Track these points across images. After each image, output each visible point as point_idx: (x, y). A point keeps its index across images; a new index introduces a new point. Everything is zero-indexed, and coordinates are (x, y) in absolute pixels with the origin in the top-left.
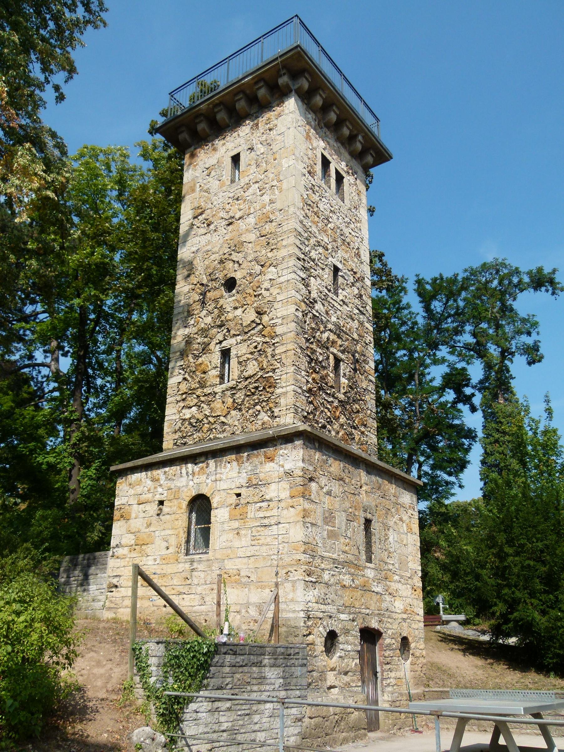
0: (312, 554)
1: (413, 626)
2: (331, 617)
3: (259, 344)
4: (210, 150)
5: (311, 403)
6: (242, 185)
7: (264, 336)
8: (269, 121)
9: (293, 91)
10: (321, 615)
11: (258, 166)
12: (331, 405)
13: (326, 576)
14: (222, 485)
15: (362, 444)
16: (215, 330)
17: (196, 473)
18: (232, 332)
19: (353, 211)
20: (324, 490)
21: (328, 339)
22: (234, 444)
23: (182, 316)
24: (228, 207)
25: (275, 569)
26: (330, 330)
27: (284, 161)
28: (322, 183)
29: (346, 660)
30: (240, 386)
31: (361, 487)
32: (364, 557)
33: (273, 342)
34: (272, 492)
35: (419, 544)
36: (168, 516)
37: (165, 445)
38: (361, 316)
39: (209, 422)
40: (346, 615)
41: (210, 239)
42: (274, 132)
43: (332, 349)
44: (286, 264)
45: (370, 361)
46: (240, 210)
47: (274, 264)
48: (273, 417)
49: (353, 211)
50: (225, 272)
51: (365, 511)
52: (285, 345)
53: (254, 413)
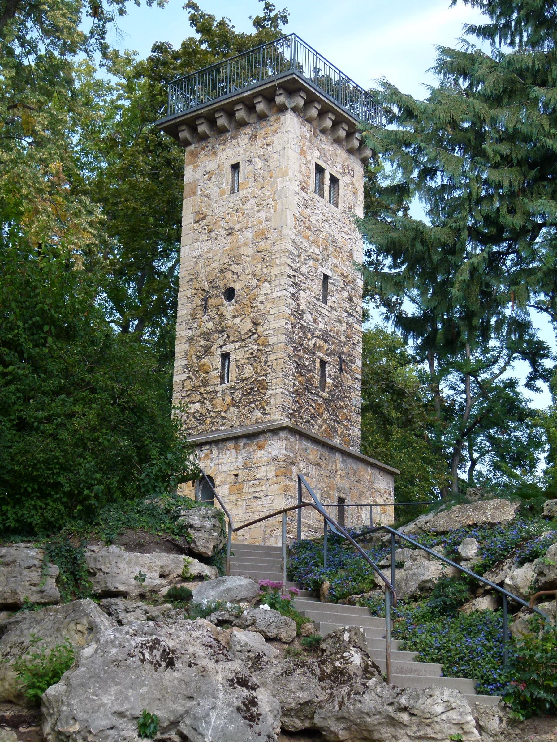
4: (211, 152)
5: (297, 402)
7: (259, 344)
8: (266, 136)
12: (315, 403)
14: (224, 468)
15: (344, 437)
17: (202, 459)
18: (232, 338)
22: (233, 435)
23: (186, 318)
25: (263, 529)
26: (317, 337)
27: (279, 180)
28: (317, 196)
31: (336, 472)
34: (262, 472)
38: (350, 319)
39: (211, 417)
41: (211, 246)
43: (318, 354)
46: (239, 222)
47: (268, 280)
48: (265, 414)
50: (226, 281)
51: (339, 491)
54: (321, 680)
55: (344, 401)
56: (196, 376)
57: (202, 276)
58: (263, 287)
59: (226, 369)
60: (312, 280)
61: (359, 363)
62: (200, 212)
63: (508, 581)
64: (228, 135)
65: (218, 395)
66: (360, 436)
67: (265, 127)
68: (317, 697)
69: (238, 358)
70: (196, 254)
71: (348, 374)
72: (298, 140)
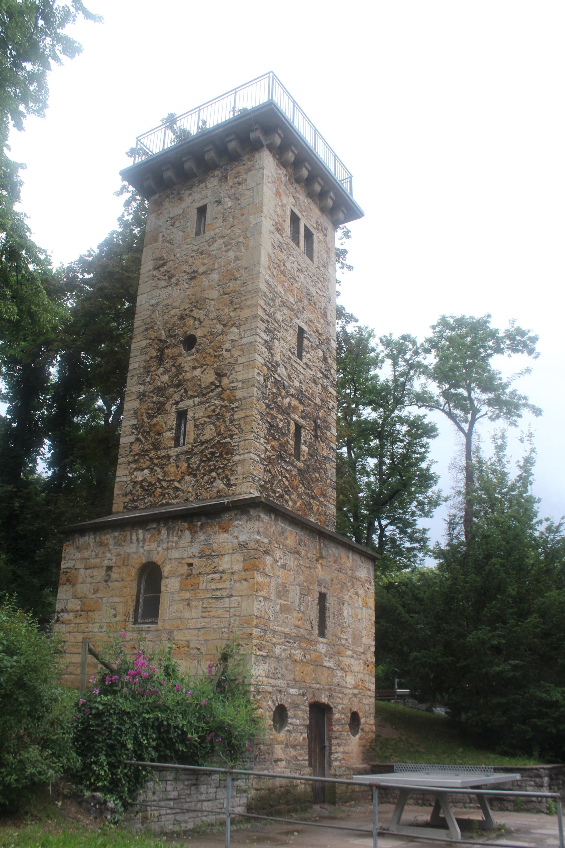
0: (263, 628)
1: (364, 701)
2: (280, 691)
3: (217, 407)
5: (269, 471)
6: (207, 238)
7: (223, 400)
9: (265, 147)
10: (270, 689)
11: (224, 220)
12: (289, 474)
13: (277, 651)
15: (320, 515)
16: (172, 390)
18: (190, 393)
19: (321, 269)
20: (279, 564)
21: (290, 404)
23: (138, 372)
24: (191, 260)
26: (292, 395)
28: (292, 244)
29: (294, 734)
30: (196, 450)
32: (317, 632)
33: (233, 406)
34: (225, 563)
35: (374, 619)
36: (116, 583)
37: (115, 508)
38: (325, 381)
39: (162, 487)
40: (296, 690)
41: (170, 292)
44: (248, 325)
45: (332, 428)
46: (204, 264)
48: (229, 485)
49: (321, 269)
50: (185, 329)
51: (320, 585)
52: (244, 411)
53: (209, 479)
55: (319, 473)
56: (146, 438)
57: (159, 324)
58: (230, 332)
59: (183, 429)
60: (287, 330)
61: (334, 431)
64: (195, 180)
65: (172, 460)
66: (335, 514)
67: (237, 166)
69: (197, 416)
70: (153, 302)
71: (323, 442)
72: (273, 179)
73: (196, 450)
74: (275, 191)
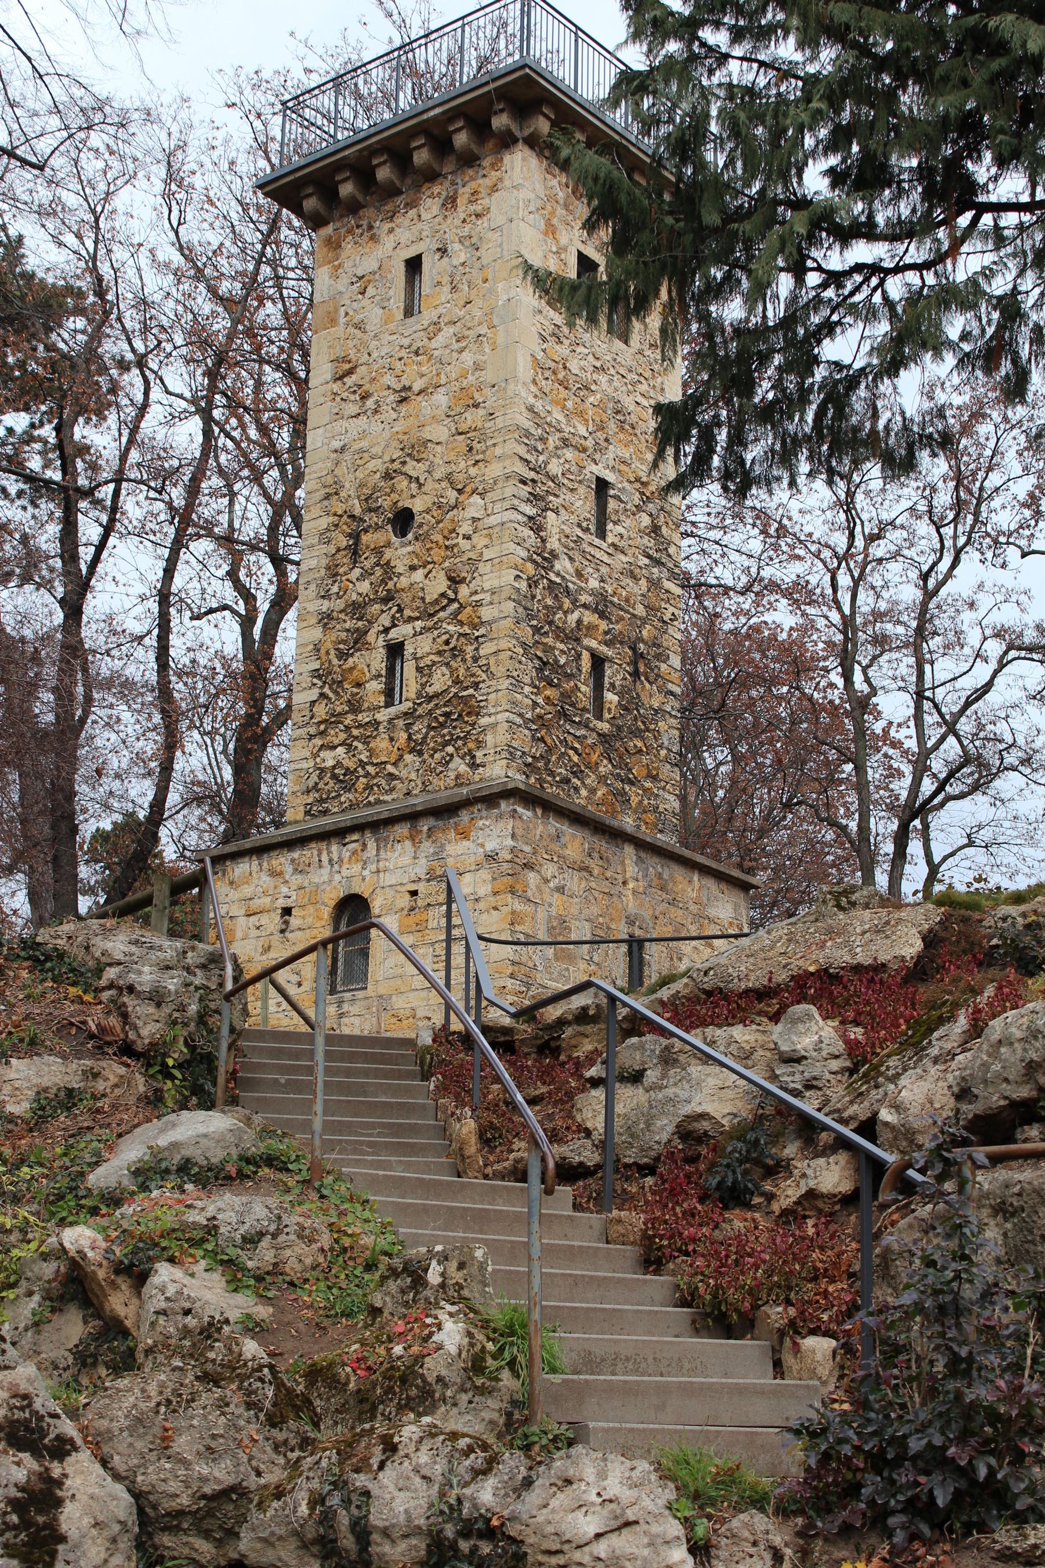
4: (365, 238)
5: (542, 740)
6: (426, 323)
7: (461, 623)
11: (454, 289)
14: (388, 879)
18: (407, 613)
21: (579, 622)
24: (398, 365)
27: (500, 286)
30: (420, 711)
31: (624, 883)
38: (655, 570)
39: (367, 775)
42: (481, 223)
43: (587, 642)
50: (395, 497)
54: (274, 1421)
55: (643, 739)
57: (349, 489)
62: (345, 359)
63: (886, 1115)
64: (400, 200)
65: (381, 729)
68: (259, 1474)
70: (337, 444)
73: (420, 711)
74: (543, 226)
